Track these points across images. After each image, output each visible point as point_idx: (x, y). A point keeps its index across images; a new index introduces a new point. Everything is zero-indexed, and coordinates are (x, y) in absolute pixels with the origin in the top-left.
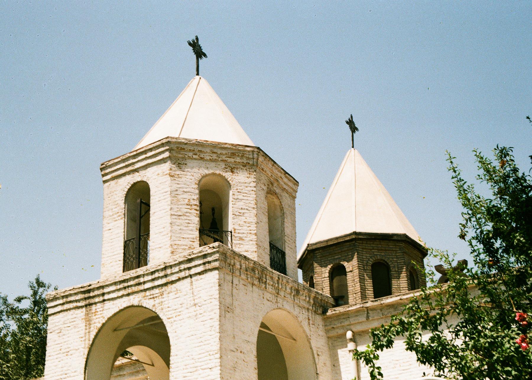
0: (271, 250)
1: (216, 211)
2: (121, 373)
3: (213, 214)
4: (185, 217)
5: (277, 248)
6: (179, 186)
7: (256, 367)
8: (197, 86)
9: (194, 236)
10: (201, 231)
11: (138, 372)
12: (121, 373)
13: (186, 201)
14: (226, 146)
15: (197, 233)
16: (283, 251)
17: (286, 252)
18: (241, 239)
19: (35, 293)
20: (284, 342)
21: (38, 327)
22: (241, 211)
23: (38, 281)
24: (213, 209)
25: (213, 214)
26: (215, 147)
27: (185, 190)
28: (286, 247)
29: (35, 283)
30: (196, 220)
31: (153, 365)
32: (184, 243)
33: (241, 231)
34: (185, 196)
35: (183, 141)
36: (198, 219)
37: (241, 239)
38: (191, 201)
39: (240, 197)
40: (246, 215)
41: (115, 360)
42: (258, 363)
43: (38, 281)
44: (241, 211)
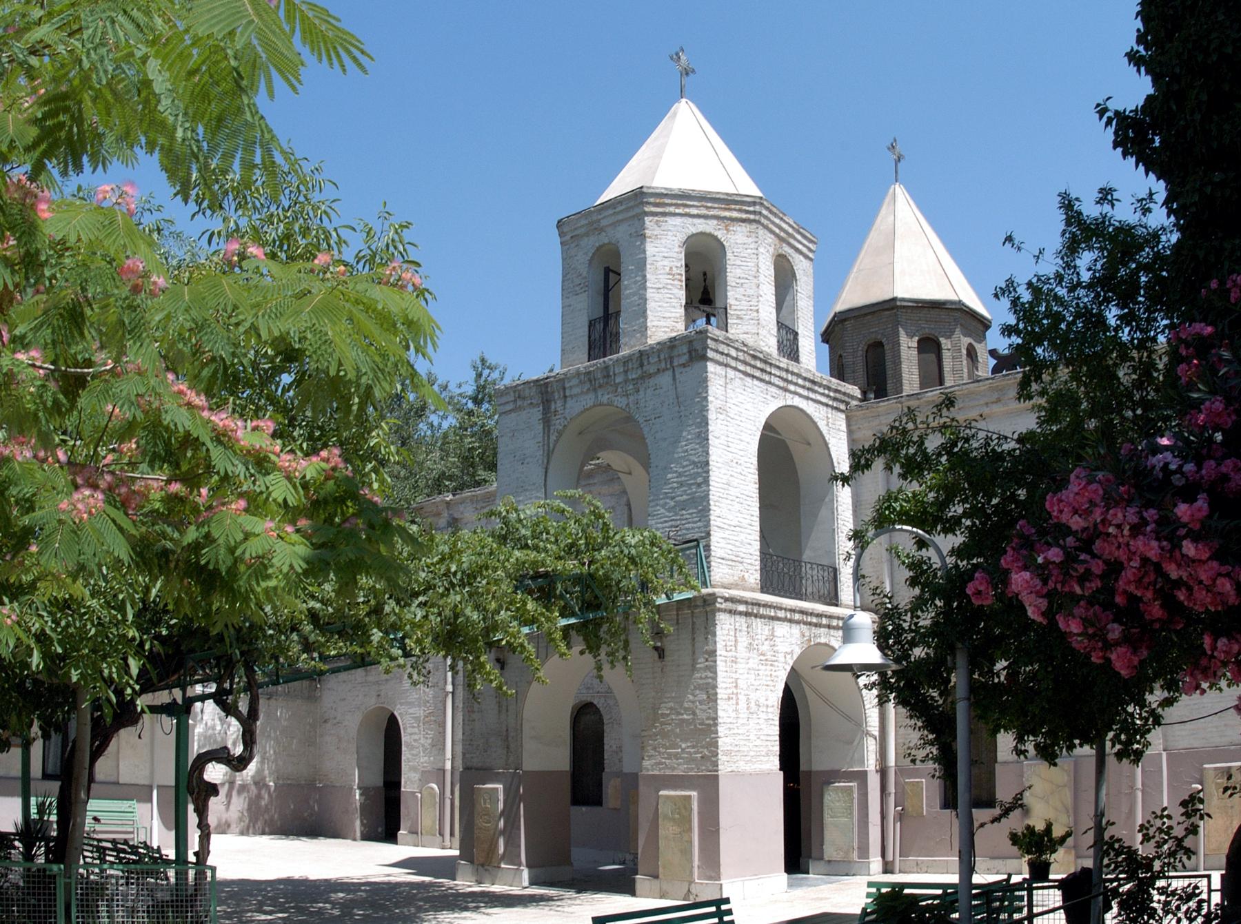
0: (779, 330)
1: (708, 276)
2: (591, 482)
3: (705, 280)
4: (666, 291)
5: (786, 326)
6: (657, 250)
7: (811, 294)
8: (546, 476)
9: (678, 315)
10: (689, 305)
11: (612, 480)
12: (591, 482)
13: (668, 269)
14: (718, 196)
15: (682, 311)
16: (794, 331)
17: (799, 332)
18: (739, 318)
19: (479, 375)
20: (796, 448)
21: (462, 471)
22: (738, 281)
23: (483, 361)
24: (705, 274)
25: (705, 280)
26: (704, 198)
27: (666, 255)
28: (800, 325)
29: (478, 362)
30: (682, 294)
31: (630, 473)
32: (665, 324)
33: (739, 308)
34: (666, 262)
35: (663, 191)
36: (683, 292)
37: (739, 318)
38: (674, 269)
39: (738, 262)
40: (745, 285)
41: (583, 465)
42: (815, 288)
43: (483, 361)
44: (738, 281)
